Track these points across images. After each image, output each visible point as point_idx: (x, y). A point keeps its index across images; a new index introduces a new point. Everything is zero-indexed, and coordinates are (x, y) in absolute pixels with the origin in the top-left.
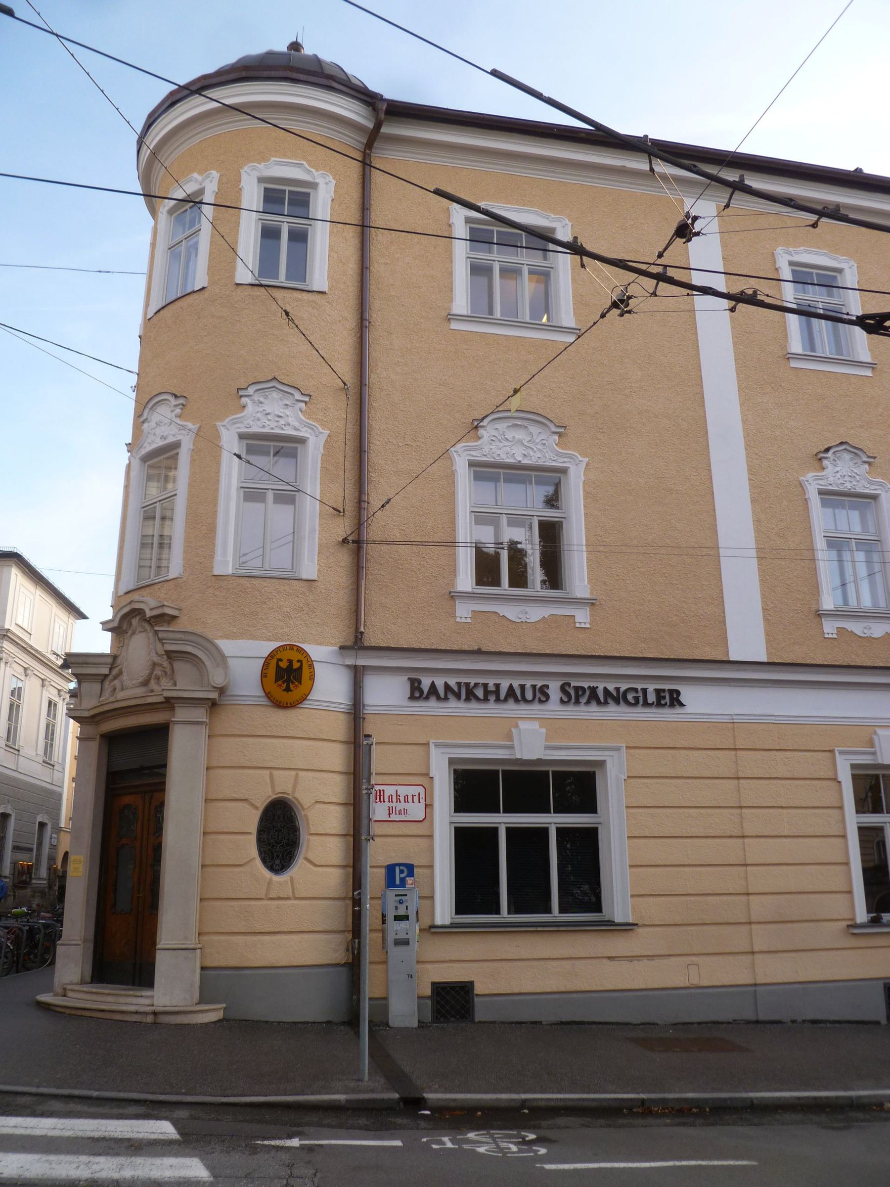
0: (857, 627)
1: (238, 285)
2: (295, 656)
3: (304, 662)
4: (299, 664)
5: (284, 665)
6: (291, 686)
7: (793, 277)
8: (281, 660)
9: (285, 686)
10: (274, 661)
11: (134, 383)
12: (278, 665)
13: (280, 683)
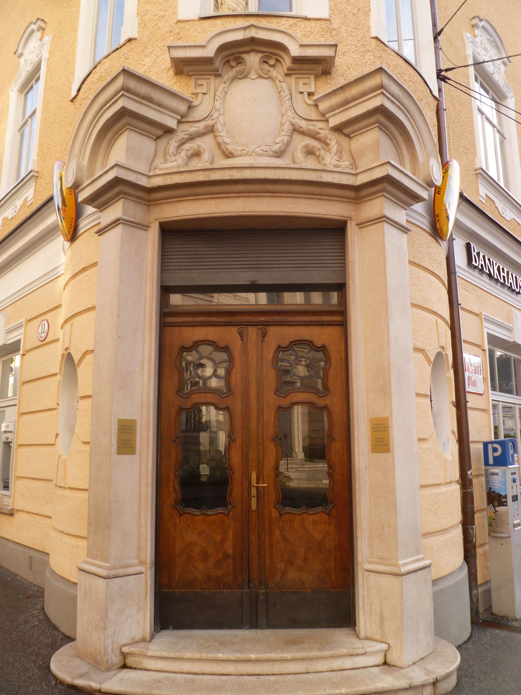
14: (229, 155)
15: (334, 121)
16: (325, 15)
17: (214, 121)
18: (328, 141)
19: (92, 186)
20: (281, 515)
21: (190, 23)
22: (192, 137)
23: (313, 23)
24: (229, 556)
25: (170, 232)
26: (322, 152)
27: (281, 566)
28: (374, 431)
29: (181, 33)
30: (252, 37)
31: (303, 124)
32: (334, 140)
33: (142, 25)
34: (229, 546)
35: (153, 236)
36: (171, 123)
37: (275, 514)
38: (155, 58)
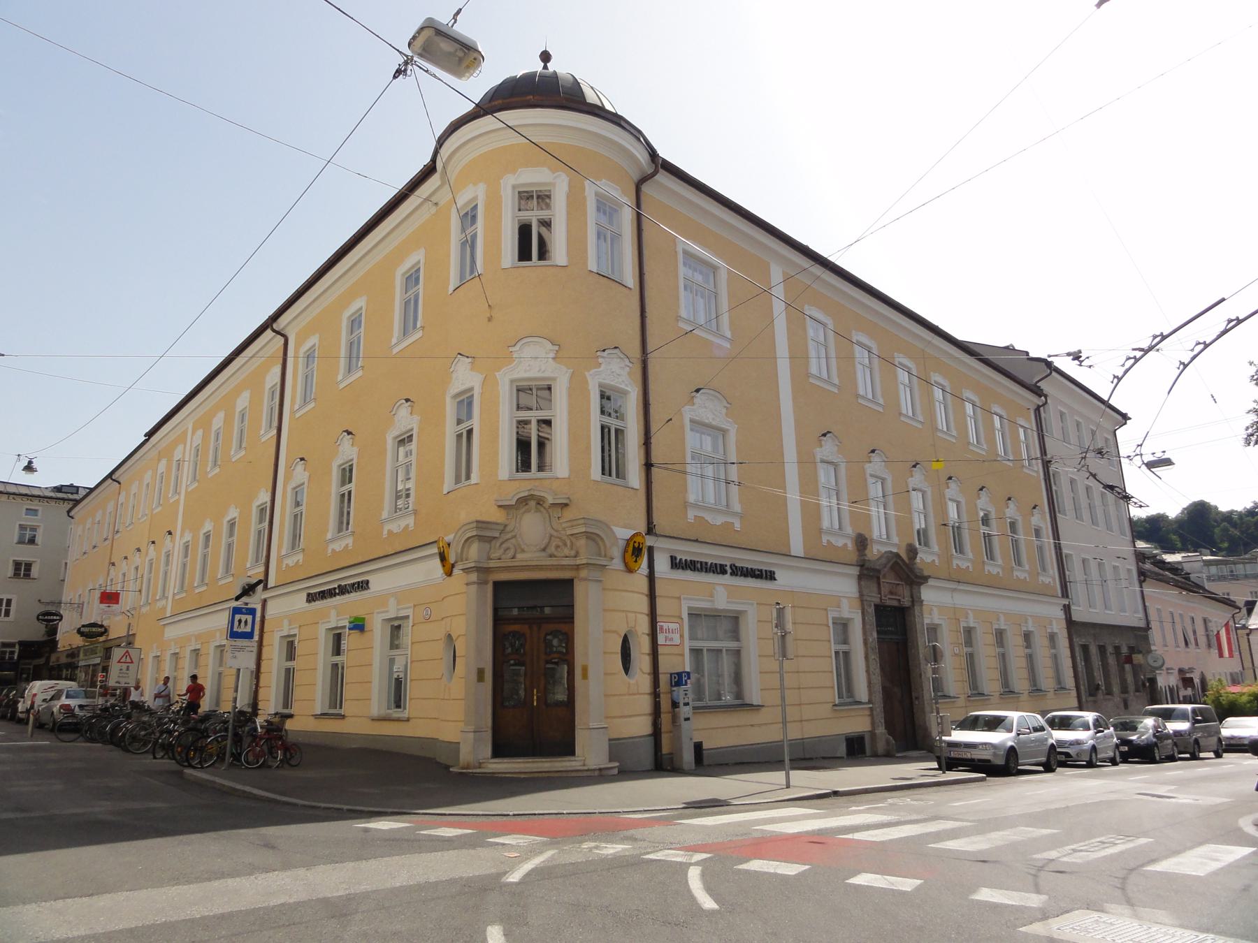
0: (709, 517)
15: (569, 532)
16: (566, 475)
25: (497, 585)
36: (497, 535)
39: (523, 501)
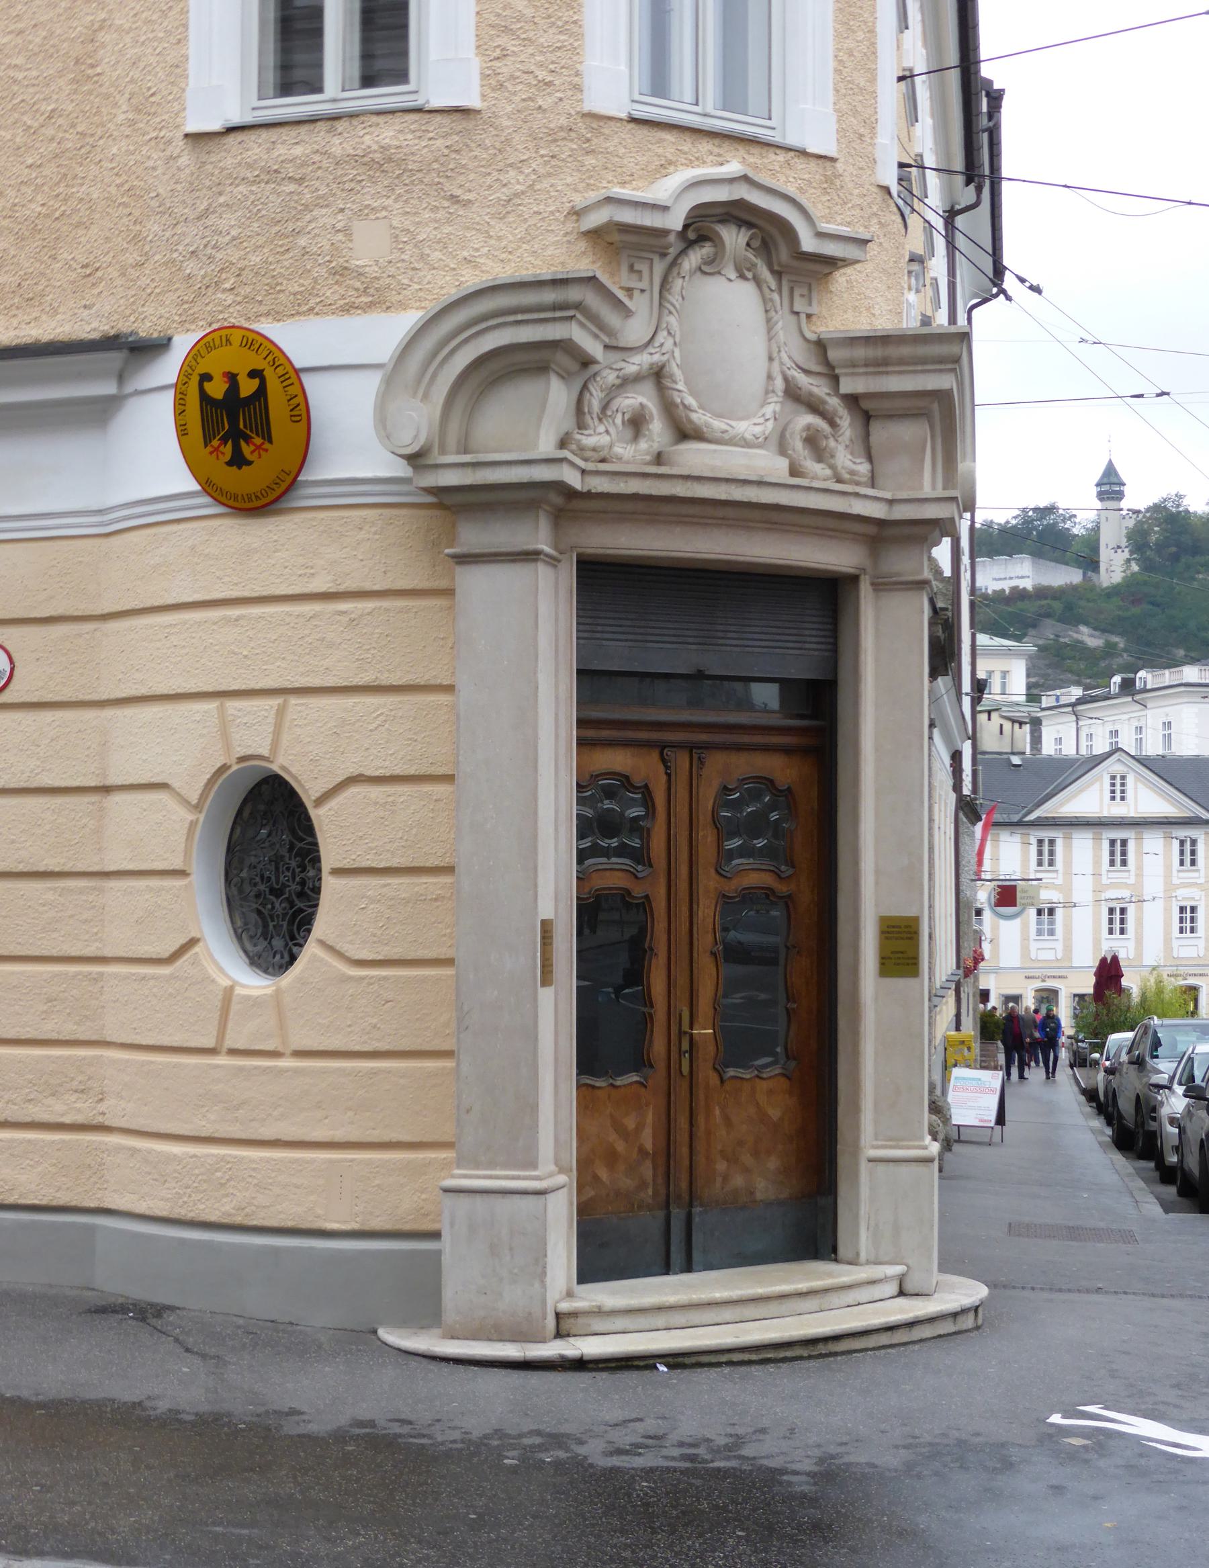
1: (1001, 1119)
2: (242, 363)
3: (269, 373)
4: (256, 382)
5: (217, 389)
6: (246, 449)
7: (938, 163)
8: (206, 377)
9: (228, 449)
10: (195, 379)
11: (1123, 980)
12: (204, 397)
13: (215, 443)
14: (685, 433)
17: (665, 358)
18: (838, 421)
19: (469, 471)
20: (722, 1081)
21: (612, 123)
22: (626, 382)
23: (813, 164)
24: (647, 1153)
26: (832, 443)
27: (721, 1166)
28: (887, 938)
29: (595, 141)
30: (742, 199)
31: (803, 380)
32: (845, 420)
33: (492, 81)
34: (647, 1139)
35: (568, 575)
37: (714, 1079)
38: (534, 177)
39: (702, 226)
